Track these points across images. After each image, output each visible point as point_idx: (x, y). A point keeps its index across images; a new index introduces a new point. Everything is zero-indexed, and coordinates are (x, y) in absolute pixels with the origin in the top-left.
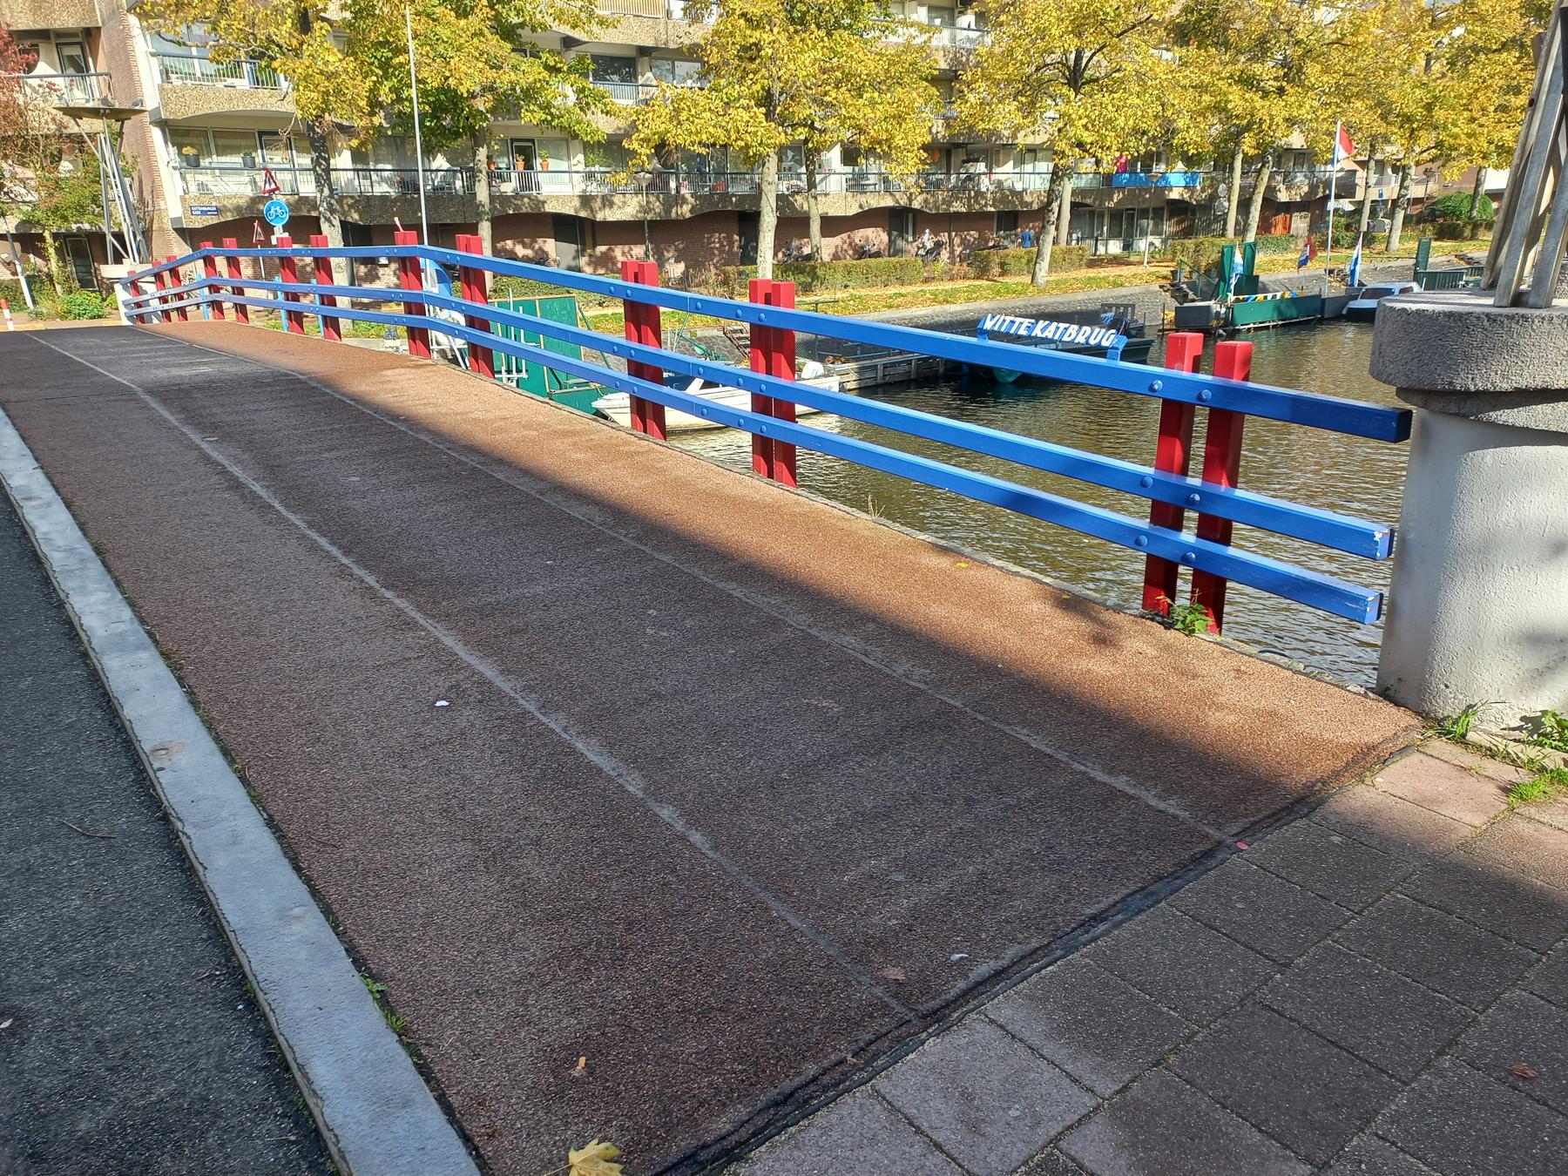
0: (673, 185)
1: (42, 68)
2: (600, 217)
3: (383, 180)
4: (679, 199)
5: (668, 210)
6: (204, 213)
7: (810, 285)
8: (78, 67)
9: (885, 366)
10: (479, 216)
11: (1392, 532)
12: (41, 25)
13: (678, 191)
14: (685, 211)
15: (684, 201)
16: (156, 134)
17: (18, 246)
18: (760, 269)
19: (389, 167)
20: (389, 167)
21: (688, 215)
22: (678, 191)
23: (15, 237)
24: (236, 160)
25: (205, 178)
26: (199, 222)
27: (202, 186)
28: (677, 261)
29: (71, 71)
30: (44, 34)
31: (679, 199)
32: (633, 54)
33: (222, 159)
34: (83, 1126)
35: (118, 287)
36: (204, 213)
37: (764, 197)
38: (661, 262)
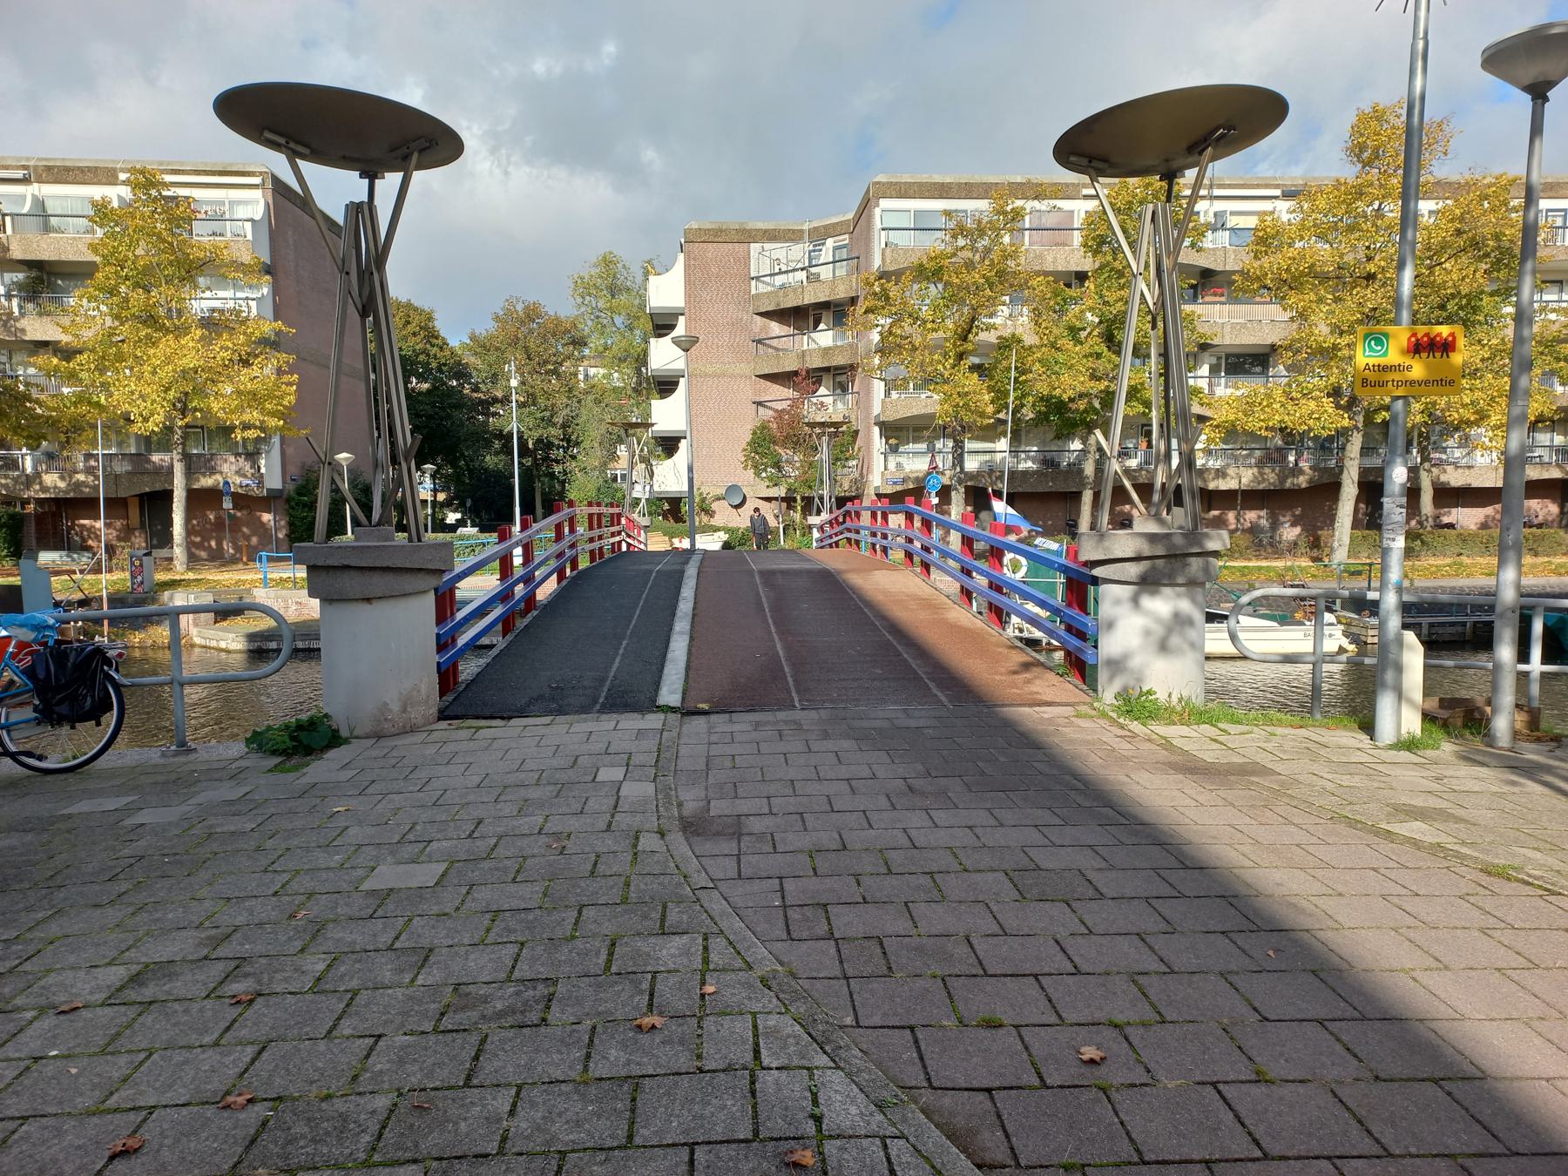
0: (1292, 458)
1: (822, 390)
2: (1212, 486)
3: (1028, 458)
4: (1296, 471)
5: (1282, 480)
6: (895, 483)
7: (299, 494)
8: (842, 388)
9: (1431, 625)
10: (1084, 485)
11: (419, 540)
12: (826, 364)
13: (1296, 464)
14: (1302, 481)
15: (1301, 472)
16: (876, 430)
17: (784, 505)
18: (1337, 533)
19: (1035, 449)
20: (1035, 449)
21: (1304, 486)
22: (1296, 464)
23: (783, 499)
24: (923, 446)
25: (902, 459)
26: (889, 490)
27: (899, 465)
28: (1293, 525)
29: (839, 391)
30: (827, 370)
31: (1296, 471)
32: (1267, 350)
33: (916, 446)
34: (212, 517)
35: (815, 530)
36: (895, 483)
37: (1345, 472)
38: (1275, 525)
